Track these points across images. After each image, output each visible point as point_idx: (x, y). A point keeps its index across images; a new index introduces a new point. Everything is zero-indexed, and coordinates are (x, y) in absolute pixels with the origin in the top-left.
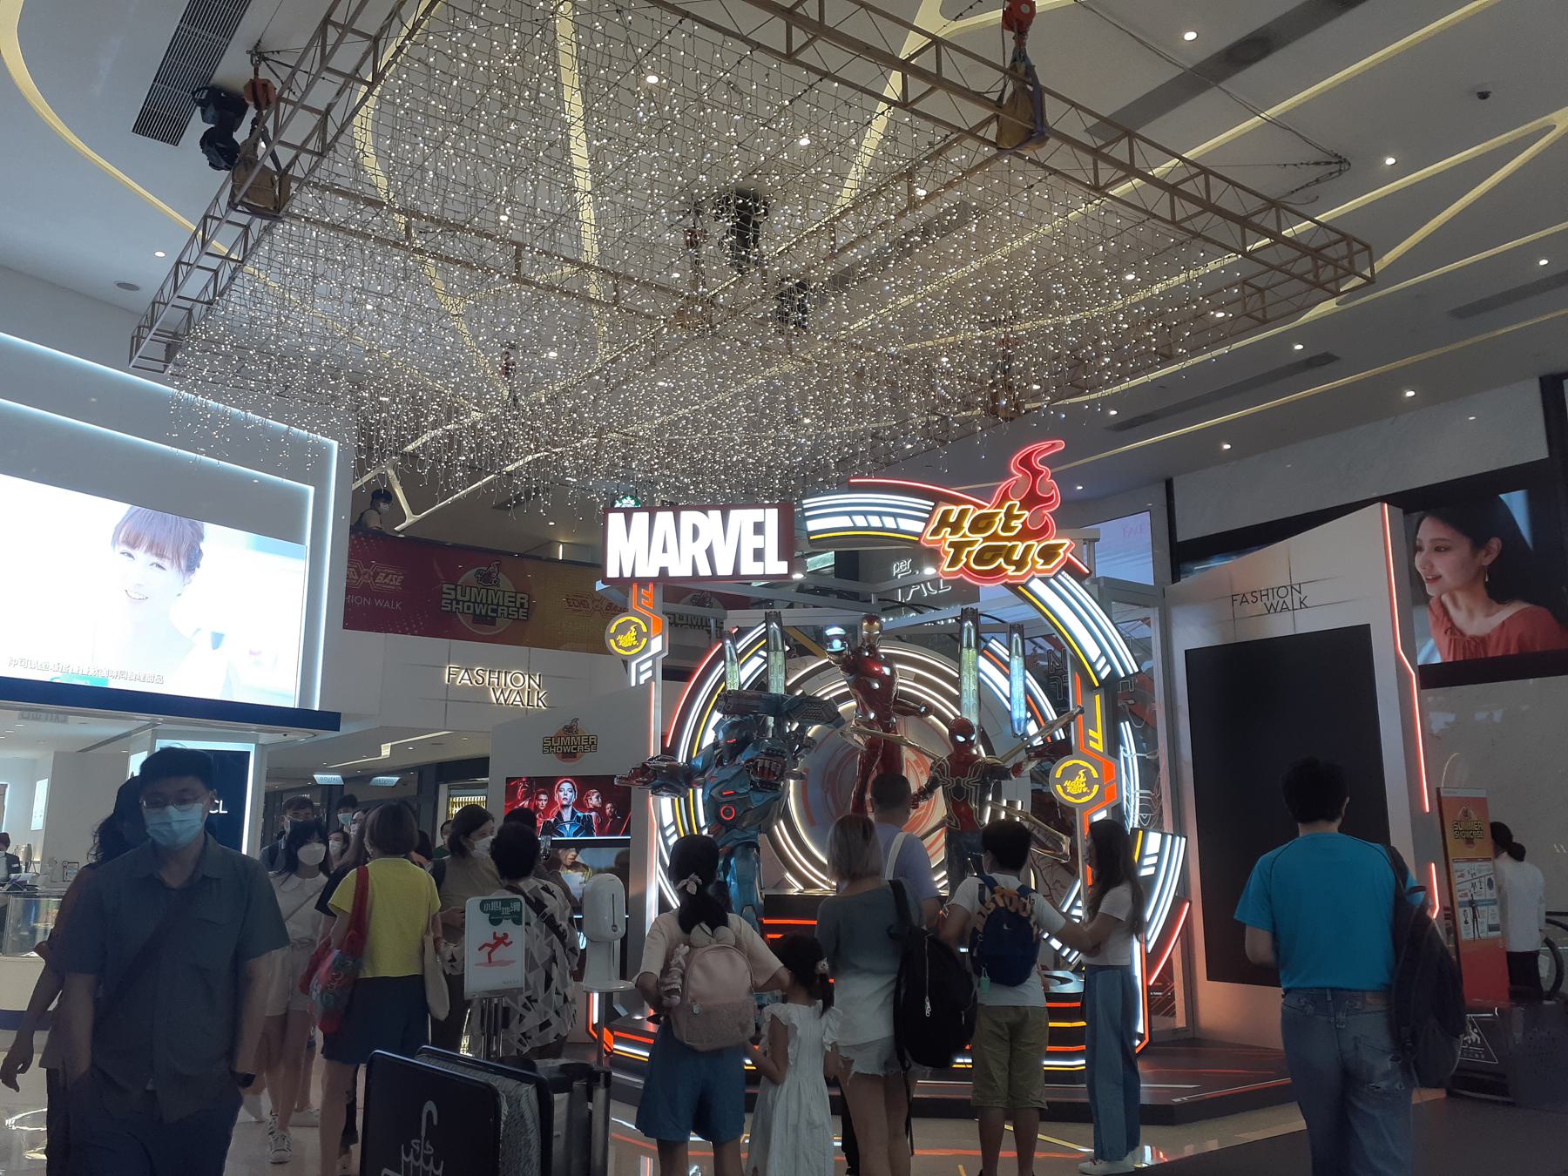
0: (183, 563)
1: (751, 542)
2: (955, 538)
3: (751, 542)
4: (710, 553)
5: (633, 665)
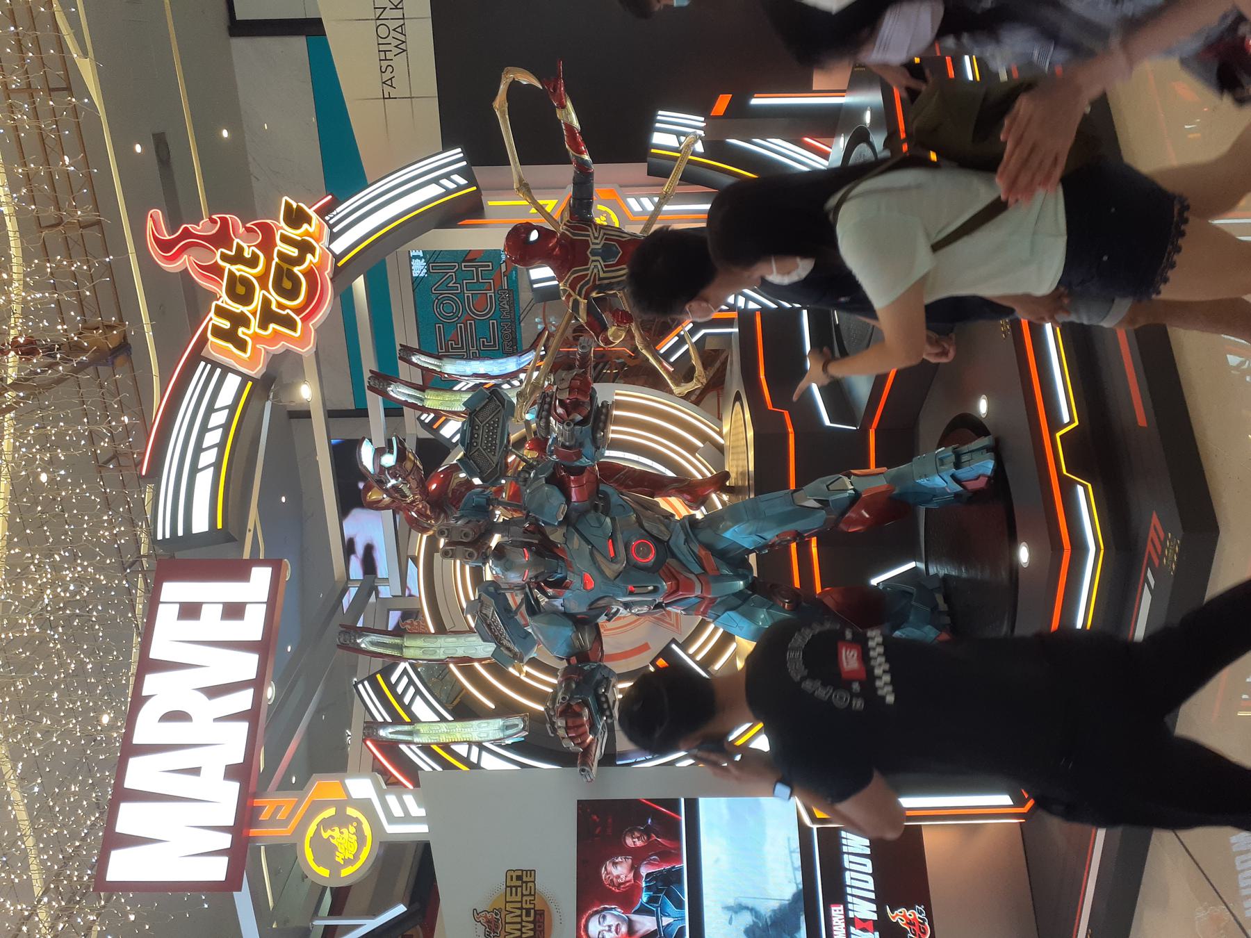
0: (723, 357)
1: (211, 624)
2: (254, 323)
3: (211, 624)
4: (214, 692)
5: (391, 829)
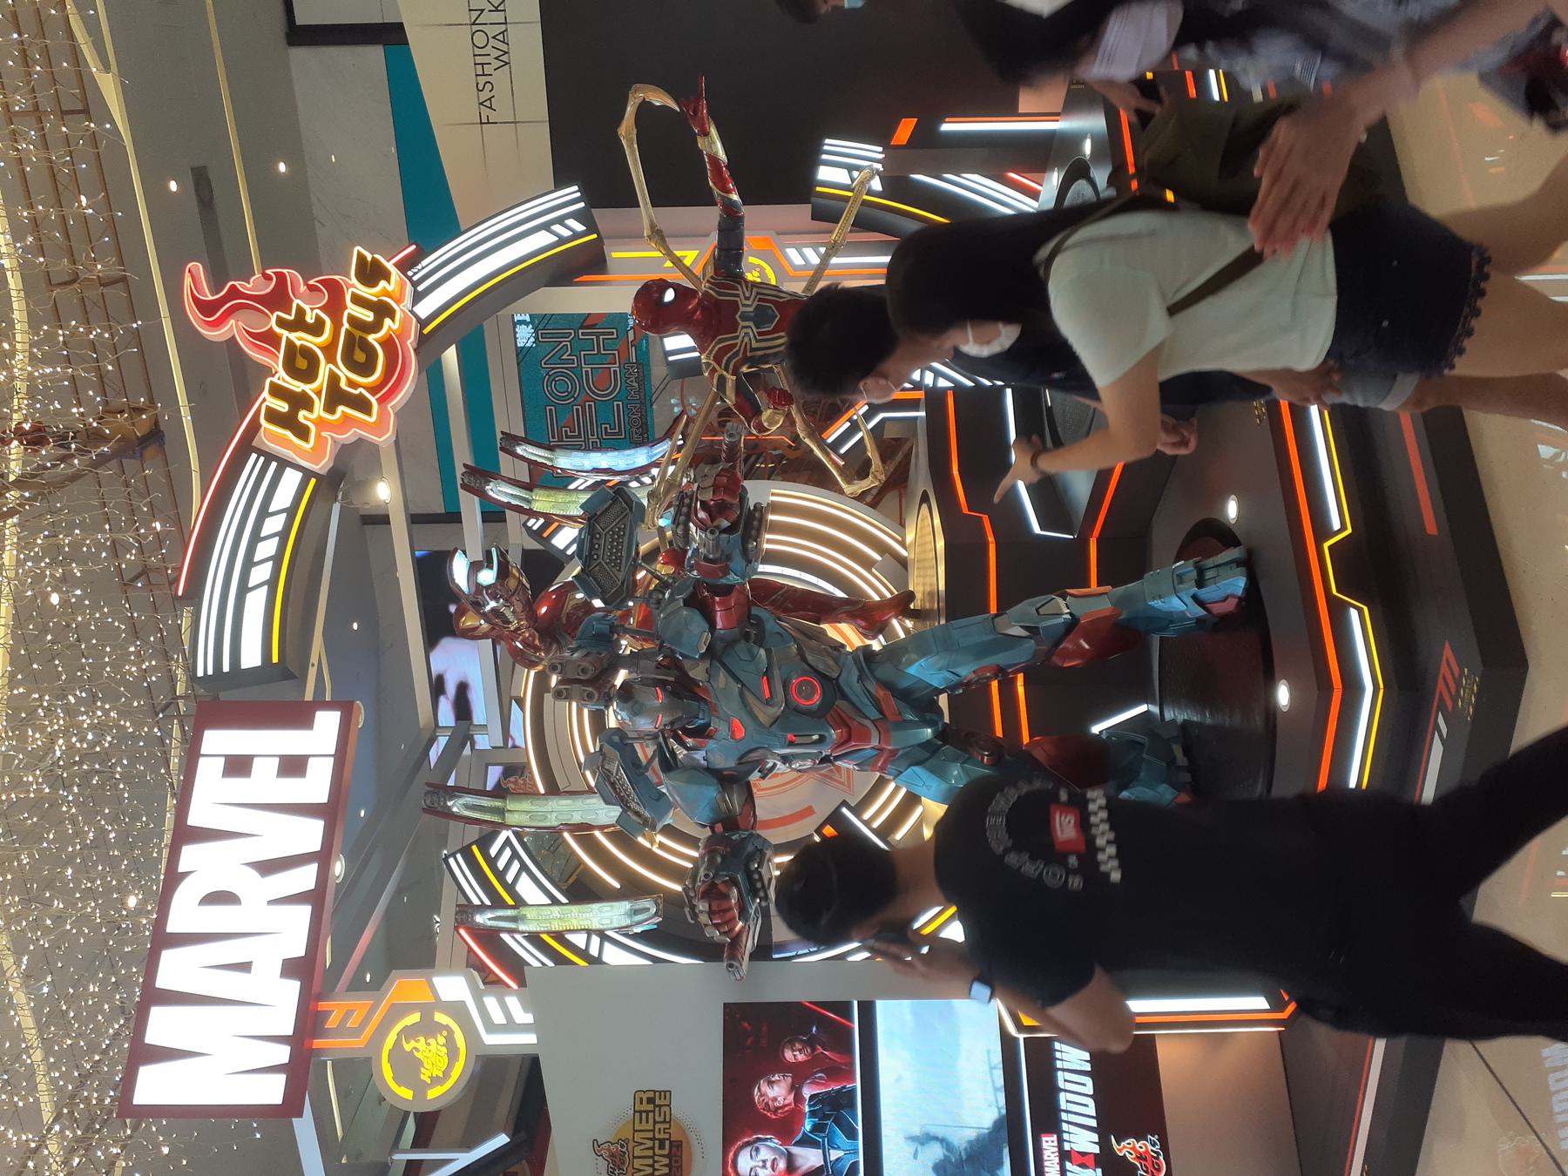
1: (265, 782)
2: (319, 405)
3: (265, 782)
4: (268, 867)
5: (490, 1039)
